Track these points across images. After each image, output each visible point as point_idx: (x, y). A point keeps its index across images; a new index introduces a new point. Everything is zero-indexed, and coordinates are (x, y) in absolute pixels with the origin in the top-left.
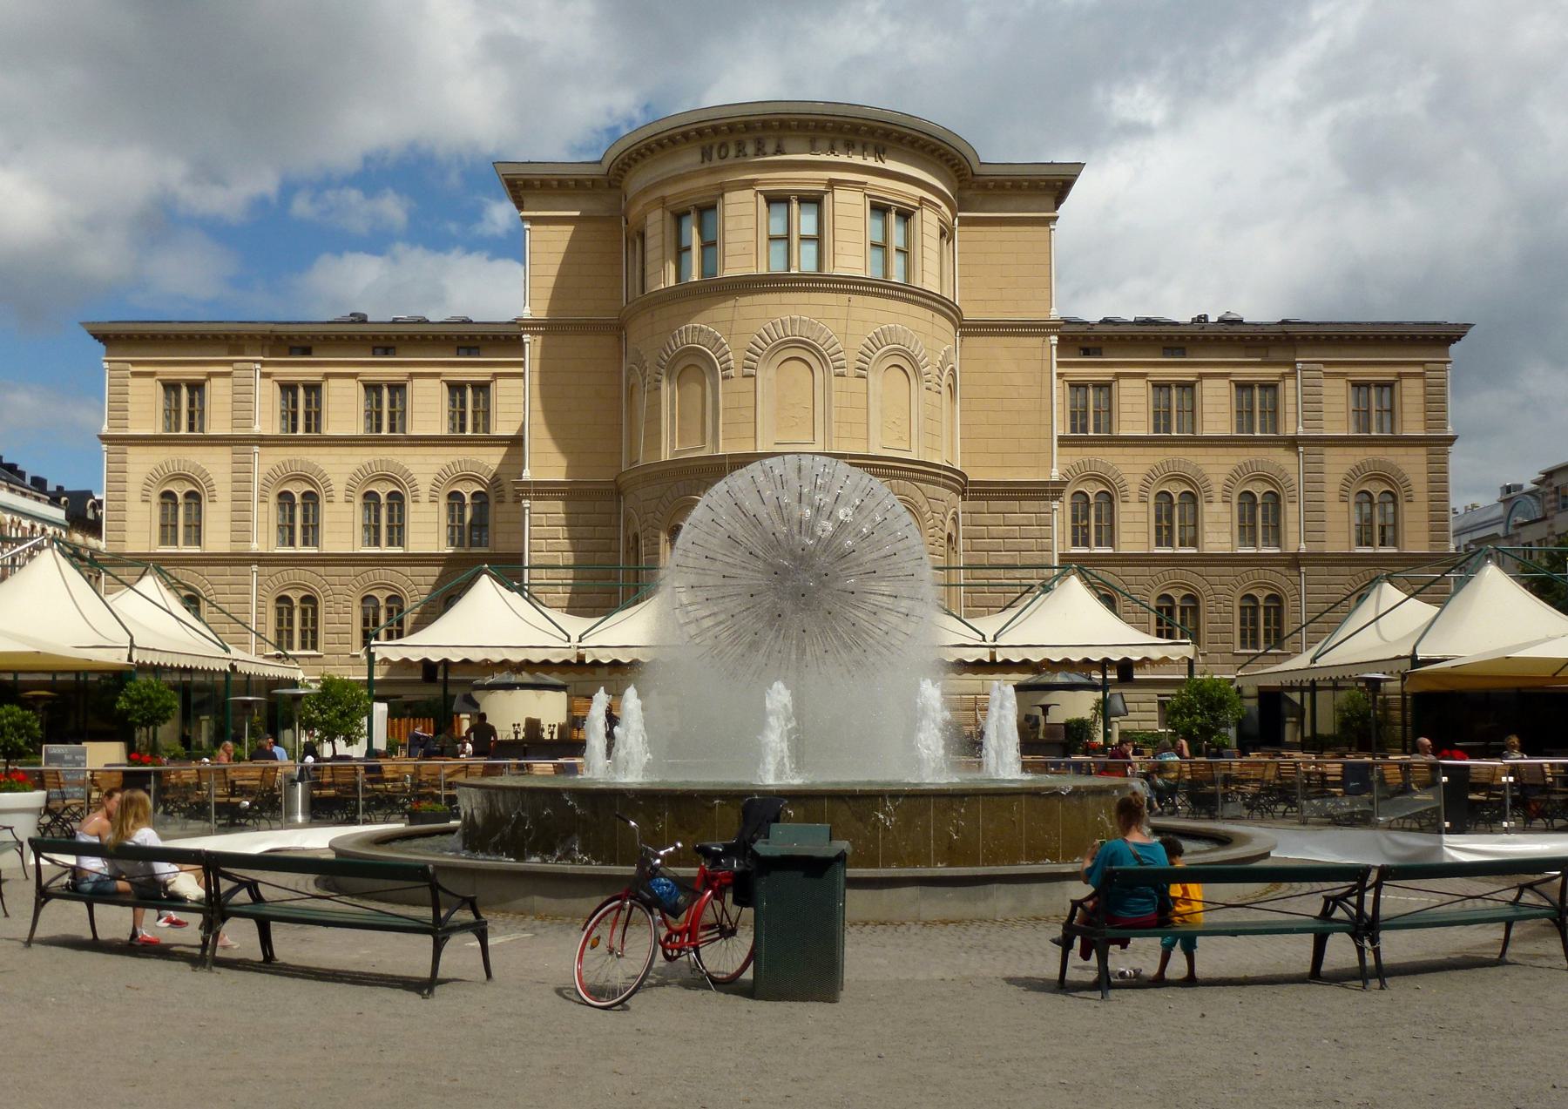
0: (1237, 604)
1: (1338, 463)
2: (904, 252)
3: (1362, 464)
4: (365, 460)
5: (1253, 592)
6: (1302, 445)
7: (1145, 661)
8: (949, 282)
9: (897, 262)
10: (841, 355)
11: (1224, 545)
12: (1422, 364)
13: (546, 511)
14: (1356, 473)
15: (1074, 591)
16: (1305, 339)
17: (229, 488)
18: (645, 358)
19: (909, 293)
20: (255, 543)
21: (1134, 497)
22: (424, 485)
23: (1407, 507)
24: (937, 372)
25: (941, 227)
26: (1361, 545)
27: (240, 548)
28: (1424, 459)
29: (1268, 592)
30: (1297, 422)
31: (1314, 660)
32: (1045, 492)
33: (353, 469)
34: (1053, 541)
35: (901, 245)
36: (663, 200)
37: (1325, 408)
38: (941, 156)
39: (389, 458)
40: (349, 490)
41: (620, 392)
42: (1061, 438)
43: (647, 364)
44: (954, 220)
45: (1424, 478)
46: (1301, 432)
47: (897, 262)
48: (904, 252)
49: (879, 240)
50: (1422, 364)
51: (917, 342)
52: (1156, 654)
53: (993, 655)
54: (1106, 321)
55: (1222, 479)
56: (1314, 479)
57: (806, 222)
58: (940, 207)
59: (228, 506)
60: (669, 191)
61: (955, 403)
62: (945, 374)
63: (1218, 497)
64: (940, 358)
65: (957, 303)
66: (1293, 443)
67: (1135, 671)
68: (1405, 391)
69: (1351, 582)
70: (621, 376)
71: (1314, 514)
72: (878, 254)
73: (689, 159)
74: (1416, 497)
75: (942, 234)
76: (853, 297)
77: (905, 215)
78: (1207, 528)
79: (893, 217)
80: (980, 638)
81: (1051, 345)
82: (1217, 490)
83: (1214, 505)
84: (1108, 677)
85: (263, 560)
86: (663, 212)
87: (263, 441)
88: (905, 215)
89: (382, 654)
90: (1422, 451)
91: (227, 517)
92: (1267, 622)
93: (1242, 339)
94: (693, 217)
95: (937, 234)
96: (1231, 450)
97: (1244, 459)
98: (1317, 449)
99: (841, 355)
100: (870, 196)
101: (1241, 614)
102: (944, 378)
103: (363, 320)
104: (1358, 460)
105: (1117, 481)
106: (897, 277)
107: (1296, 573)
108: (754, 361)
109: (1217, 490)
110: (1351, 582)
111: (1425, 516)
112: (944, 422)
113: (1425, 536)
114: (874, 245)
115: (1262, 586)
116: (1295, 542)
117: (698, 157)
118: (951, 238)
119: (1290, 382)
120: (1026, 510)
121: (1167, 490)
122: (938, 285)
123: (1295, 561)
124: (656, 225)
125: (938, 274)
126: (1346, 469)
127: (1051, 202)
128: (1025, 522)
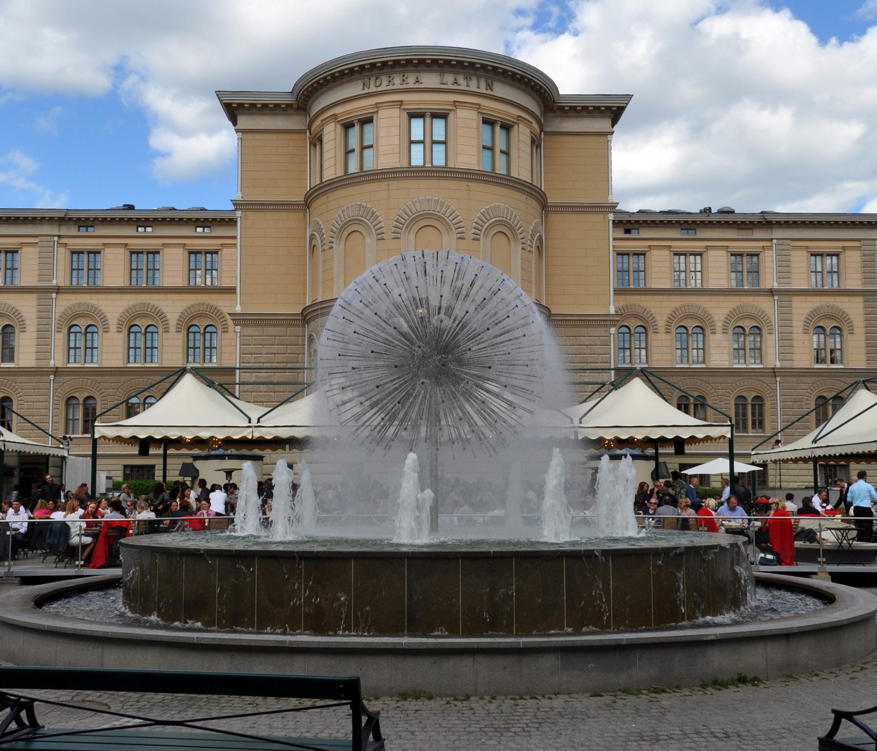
0: (733, 403)
1: (802, 308)
2: (507, 153)
3: (811, 312)
4: (132, 303)
5: (744, 394)
6: (777, 295)
7: (693, 439)
8: (537, 177)
9: (501, 160)
10: (461, 224)
11: (724, 362)
12: (859, 240)
13: (252, 334)
14: (814, 314)
15: (637, 387)
16: (778, 223)
17: (35, 322)
18: (322, 227)
19: (508, 182)
20: (52, 360)
21: (661, 329)
22: (173, 318)
23: (850, 337)
24: (529, 242)
25: (532, 137)
26: (818, 362)
27: (43, 364)
28: (861, 305)
29: (754, 394)
30: (774, 279)
31: (815, 441)
32: (604, 321)
33: (122, 309)
34: (610, 357)
35: (504, 148)
36: (335, 116)
37: (793, 270)
38: (532, 87)
39: (148, 302)
40: (120, 324)
41: (305, 251)
42: (615, 290)
43: (324, 231)
44: (541, 133)
45: (861, 318)
46: (776, 286)
47: (501, 160)
48: (507, 153)
49: (489, 144)
50: (859, 240)
51: (516, 217)
52: (700, 434)
53: (576, 433)
54: (640, 212)
55: (722, 318)
56: (786, 319)
57: (439, 126)
58: (531, 123)
59: (34, 335)
60: (337, 110)
61: (542, 259)
62: (535, 239)
63: (719, 330)
64: (532, 228)
65: (543, 190)
66: (772, 292)
67: (686, 447)
68: (848, 259)
69: (812, 387)
70: (306, 241)
71: (786, 340)
72: (488, 153)
73: (354, 89)
74: (856, 331)
75: (533, 141)
76: (471, 184)
77: (507, 127)
78: (712, 351)
79: (498, 129)
80: (569, 420)
81: (609, 221)
82: (719, 325)
83: (717, 335)
84: (660, 451)
85: (56, 371)
86: (335, 125)
87: (58, 290)
88: (507, 127)
89: (100, 432)
90: (860, 299)
91: (34, 342)
92: (753, 414)
93: (735, 222)
94: (357, 128)
95: (529, 141)
96: (728, 298)
97: (736, 304)
98: (787, 298)
99: (461, 224)
100: (482, 113)
101: (735, 408)
102: (534, 242)
103: (131, 207)
104: (815, 305)
105: (650, 319)
106: (501, 169)
107: (774, 381)
108: (400, 228)
109: (719, 325)
110: (812, 387)
111: (863, 344)
112: (533, 272)
113: (863, 357)
114: (484, 147)
115: (750, 390)
116: (773, 360)
117: (361, 87)
118: (538, 146)
119: (768, 253)
120: (592, 334)
121: (684, 325)
122: (530, 178)
123: (774, 372)
124: (331, 133)
125: (530, 170)
126: (807, 311)
127: (608, 122)
128: (591, 343)
